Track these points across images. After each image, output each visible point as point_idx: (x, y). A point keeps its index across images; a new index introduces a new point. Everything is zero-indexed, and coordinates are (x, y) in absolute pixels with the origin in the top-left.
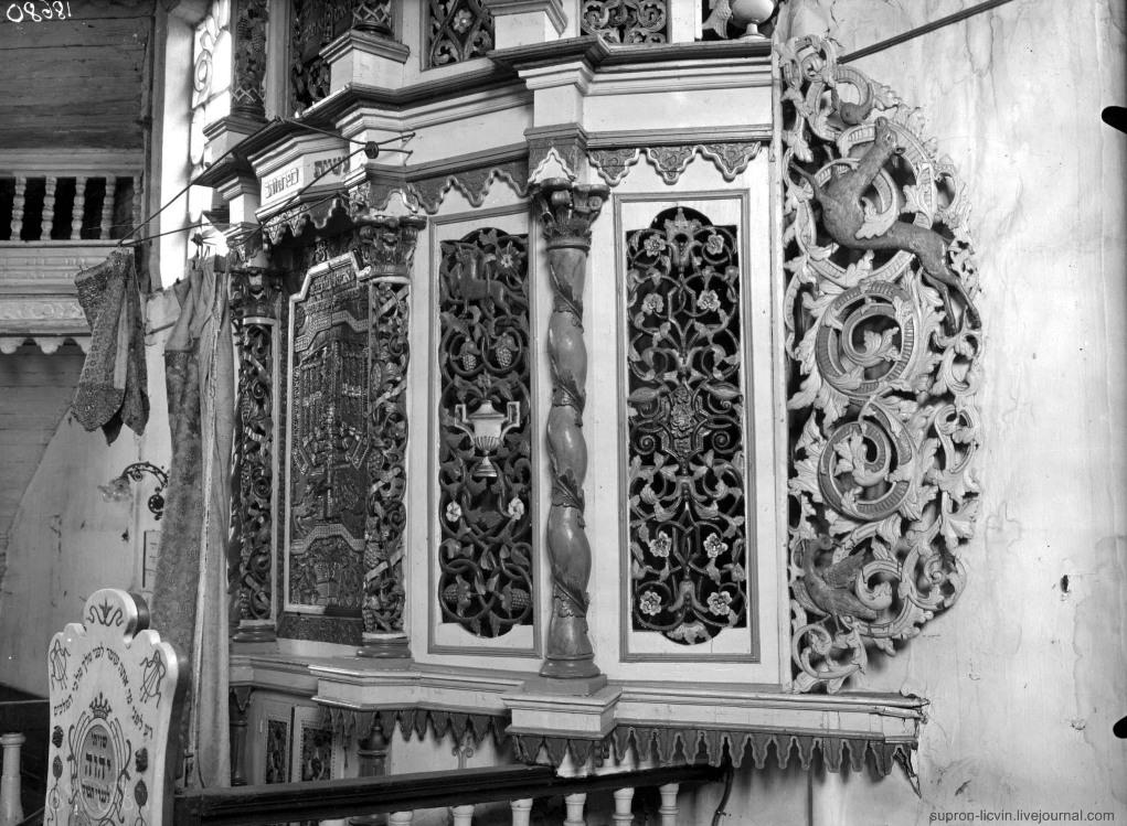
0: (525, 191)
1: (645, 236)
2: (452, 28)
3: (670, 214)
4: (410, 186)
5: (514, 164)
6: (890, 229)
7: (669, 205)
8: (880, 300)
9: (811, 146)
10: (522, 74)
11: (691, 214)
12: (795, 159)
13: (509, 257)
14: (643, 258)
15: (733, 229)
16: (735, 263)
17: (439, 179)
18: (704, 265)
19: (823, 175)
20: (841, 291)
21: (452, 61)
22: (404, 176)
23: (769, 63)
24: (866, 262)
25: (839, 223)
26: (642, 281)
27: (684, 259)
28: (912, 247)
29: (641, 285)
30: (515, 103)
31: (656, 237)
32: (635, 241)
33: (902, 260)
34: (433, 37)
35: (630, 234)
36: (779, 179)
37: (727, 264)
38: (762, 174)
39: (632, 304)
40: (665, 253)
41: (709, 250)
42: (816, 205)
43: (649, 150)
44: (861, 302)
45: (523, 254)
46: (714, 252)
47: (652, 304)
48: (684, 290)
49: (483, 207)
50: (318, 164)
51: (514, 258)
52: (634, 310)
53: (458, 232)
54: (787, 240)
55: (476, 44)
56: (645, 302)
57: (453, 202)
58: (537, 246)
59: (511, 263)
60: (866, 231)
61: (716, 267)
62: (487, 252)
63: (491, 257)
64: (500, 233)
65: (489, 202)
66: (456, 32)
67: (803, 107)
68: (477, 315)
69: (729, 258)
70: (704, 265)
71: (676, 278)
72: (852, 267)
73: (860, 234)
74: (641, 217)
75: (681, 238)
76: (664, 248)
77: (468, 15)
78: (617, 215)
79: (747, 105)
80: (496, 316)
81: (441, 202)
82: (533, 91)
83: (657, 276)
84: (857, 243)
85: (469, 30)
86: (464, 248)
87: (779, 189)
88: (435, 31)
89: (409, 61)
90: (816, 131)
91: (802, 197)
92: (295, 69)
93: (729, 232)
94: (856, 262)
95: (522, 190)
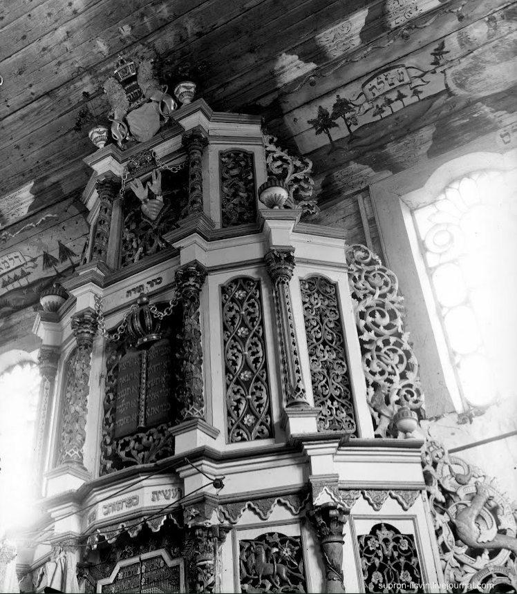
0: (298, 512)
1: (367, 539)
2: (243, 424)
3: (378, 527)
4: (221, 507)
5: (291, 496)
6: (495, 537)
7: (378, 522)
8: (499, 575)
9: (443, 494)
10: (305, 447)
11: (389, 527)
12: (435, 500)
13: (288, 549)
14: (368, 551)
15: (411, 536)
16: (416, 556)
17: (241, 504)
18: (399, 557)
19: (452, 509)
20: (475, 571)
21: (243, 440)
22: (218, 501)
23: (420, 452)
24: (486, 555)
25: (467, 534)
26: (369, 564)
27: (390, 553)
28: (509, 547)
29: (369, 566)
30: (293, 463)
31: (373, 539)
32: (363, 541)
33: (504, 555)
34: (230, 427)
35: (359, 537)
36: (429, 511)
37: (411, 555)
38: (421, 506)
39: (366, 578)
40: (378, 548)
41: (401, 547)
42: (453, 527)
43: (366, 492)
44: (490, 577)
45: (297, 548)
46: (403, 549)
47: (377, 577)
48: (392, 570)
49: (269, 520)
50: (154, 493)
51: (292, 551)
52: (368, 581)
53: (252, 535)
54: (440, 543)
55: (259, 432)
56: (373, 576)
57: (247, 517)
58: (308, 542)
59: (290, 553)
60: (483, 539)
61: (406, 557)
62: (273, 547)
63: (275, 550)
64: (280, 535)
65: (272, 518)
66: (246, 426)
67: (436, 475)
68: (269, 586)
69: (412, 553)
70: (399, 557)
71: (387, 563)
72: (479, 558)
73: (480, 540)
74: (364, 528)
75: (386, 541)
76: (378, 546)
77: (253, 417)
78: (352, 526)
79: (408, 471)
80: (281, 585)
81: (271, 512)
82: (310, 456)
83: (377, 562)
84: (479, 545)
85: (253, 425)
86: (256, 544)
87: (430, 516)
88: (232, 424)
89: (218, 438)
90: (445, 487)
91: (445, 520)
92: (105, 442)
93: (410, 538)
94: (481, 556)
95: (296, 511)
